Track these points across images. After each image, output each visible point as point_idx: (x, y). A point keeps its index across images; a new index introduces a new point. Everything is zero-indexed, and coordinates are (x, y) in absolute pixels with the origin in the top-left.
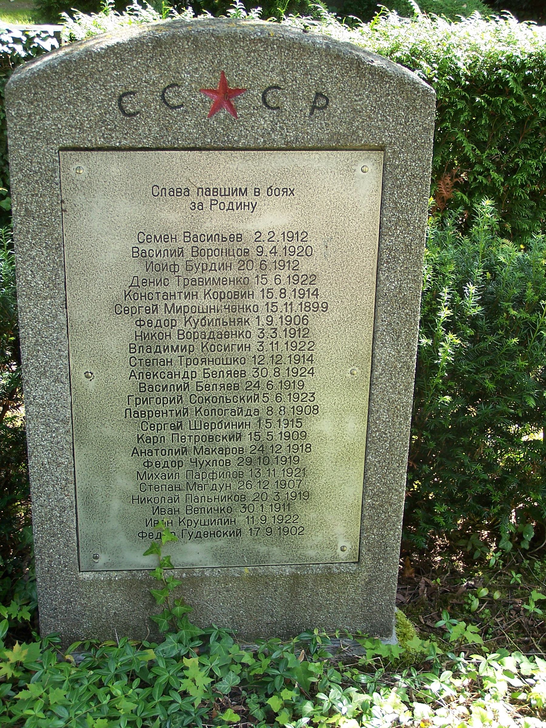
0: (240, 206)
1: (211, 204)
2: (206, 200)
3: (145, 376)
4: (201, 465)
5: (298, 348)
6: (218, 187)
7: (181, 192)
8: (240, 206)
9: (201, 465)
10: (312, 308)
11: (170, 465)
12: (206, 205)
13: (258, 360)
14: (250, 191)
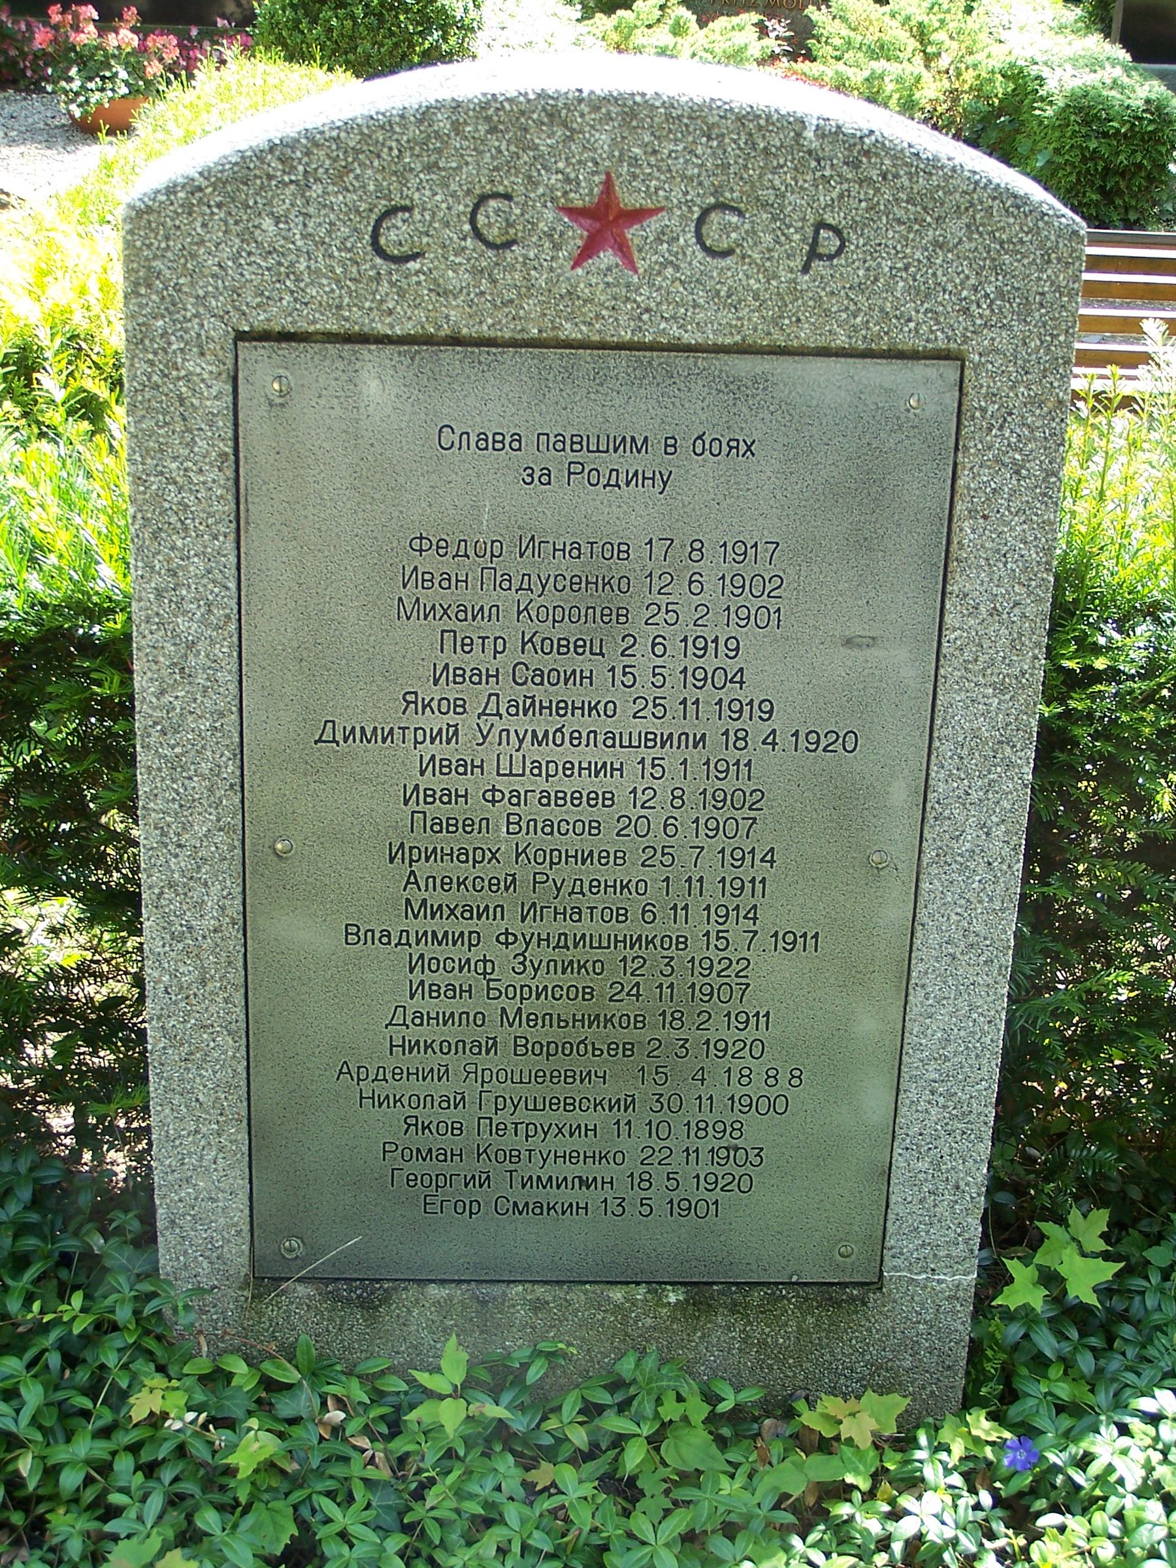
1: (570, 473)
2: (554, 460)
11: (389, 1076)
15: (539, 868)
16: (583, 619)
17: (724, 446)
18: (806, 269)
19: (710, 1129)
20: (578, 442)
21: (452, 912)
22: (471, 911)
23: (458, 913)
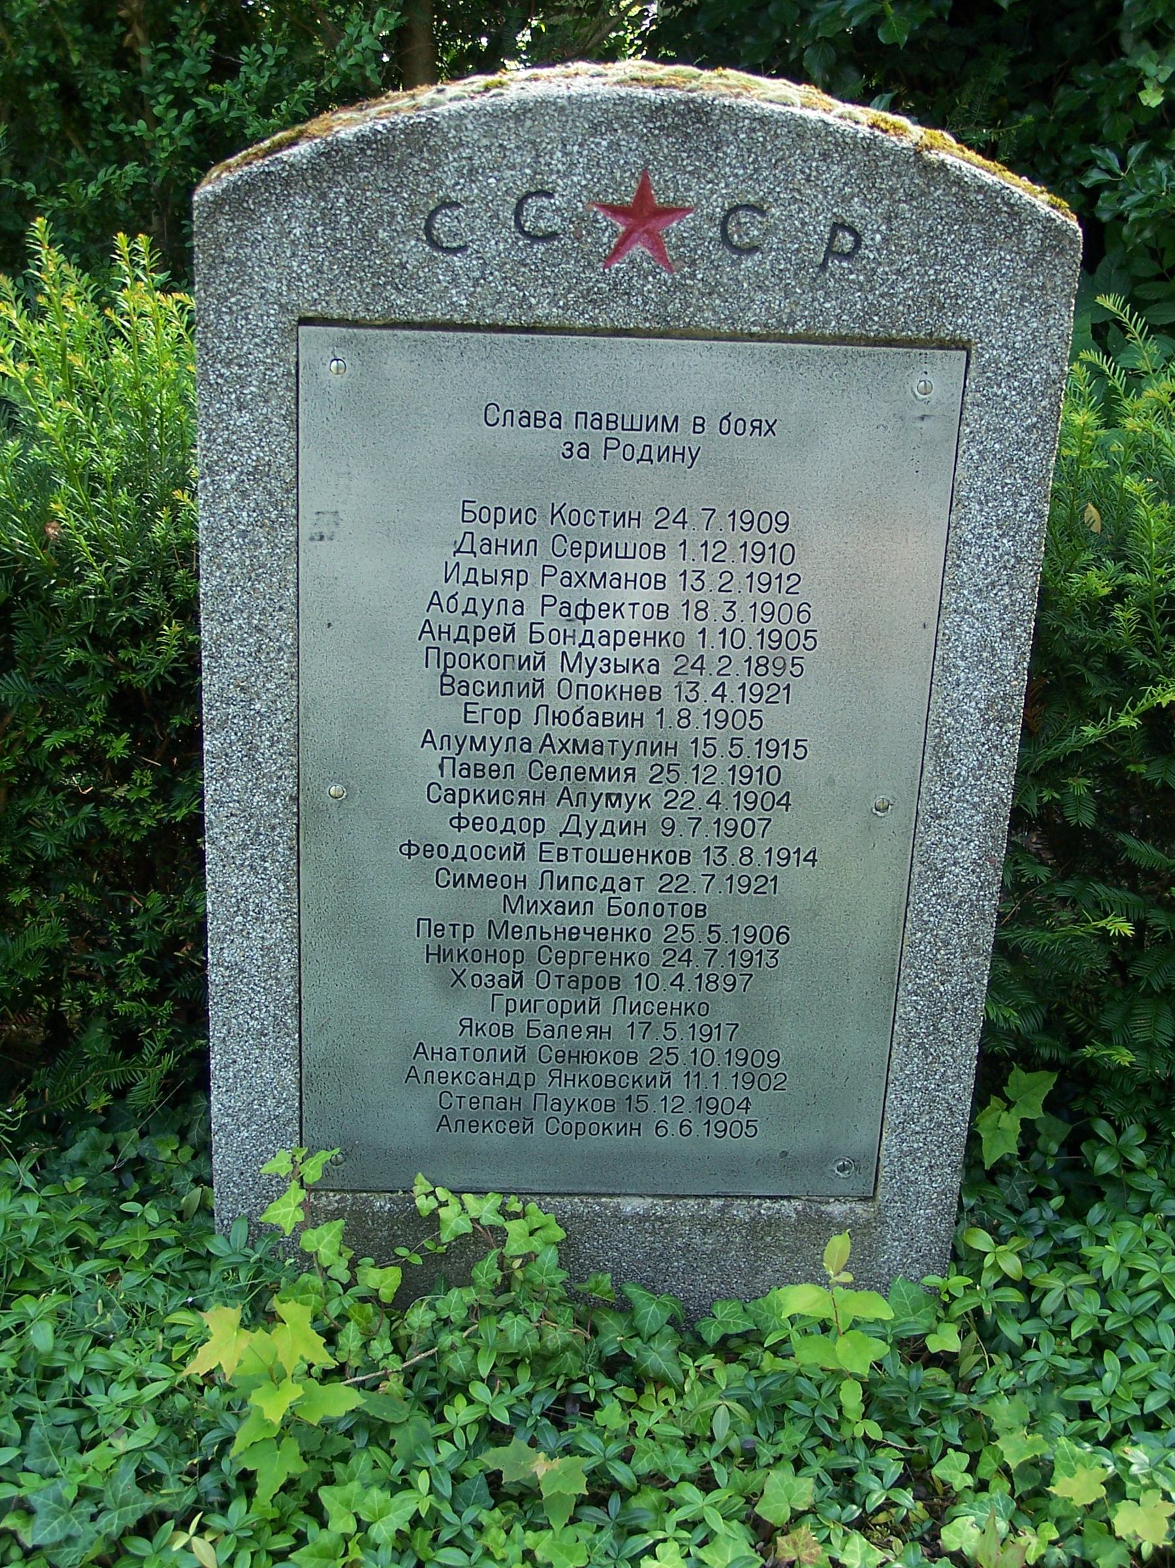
0: (665, 453)
2: (597, 439)
3: (516, 421)
8: (665, 453)
12: (597, 448)
13: (712, 552)
14: (685, 424)
17: (748, 426)
20: (612, 421)
23: (551, 908)
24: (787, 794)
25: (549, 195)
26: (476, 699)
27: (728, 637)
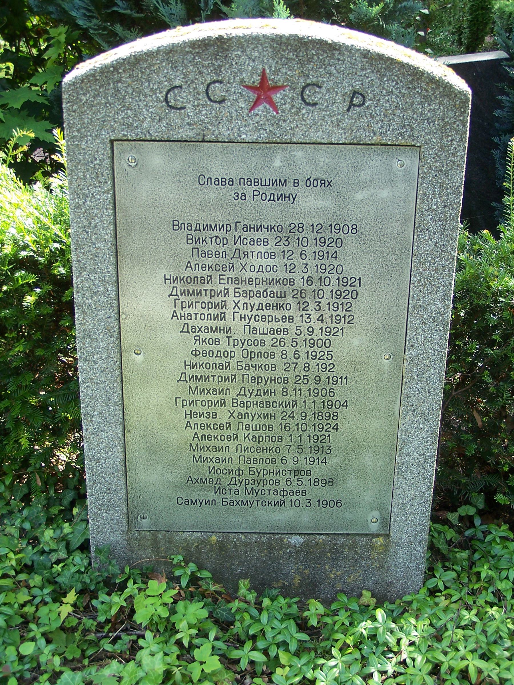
1: (254, 195)
2: (249, 190)
4: (253, 417)
5: (328, 369)
6: (259, 178)
7: (225, 182)
9: (253, 417)
10: (324, 417)
15: (189, 232)
16: (206, 318)
18: (348, 110)
19: (324, 415)
20: (256, 182)
21: (209, 392)
22: (216, 391)
23: (211, 391)
24: (346, 401)
25: (320, 87)
26: (224, 273)
27: (300, 427)
